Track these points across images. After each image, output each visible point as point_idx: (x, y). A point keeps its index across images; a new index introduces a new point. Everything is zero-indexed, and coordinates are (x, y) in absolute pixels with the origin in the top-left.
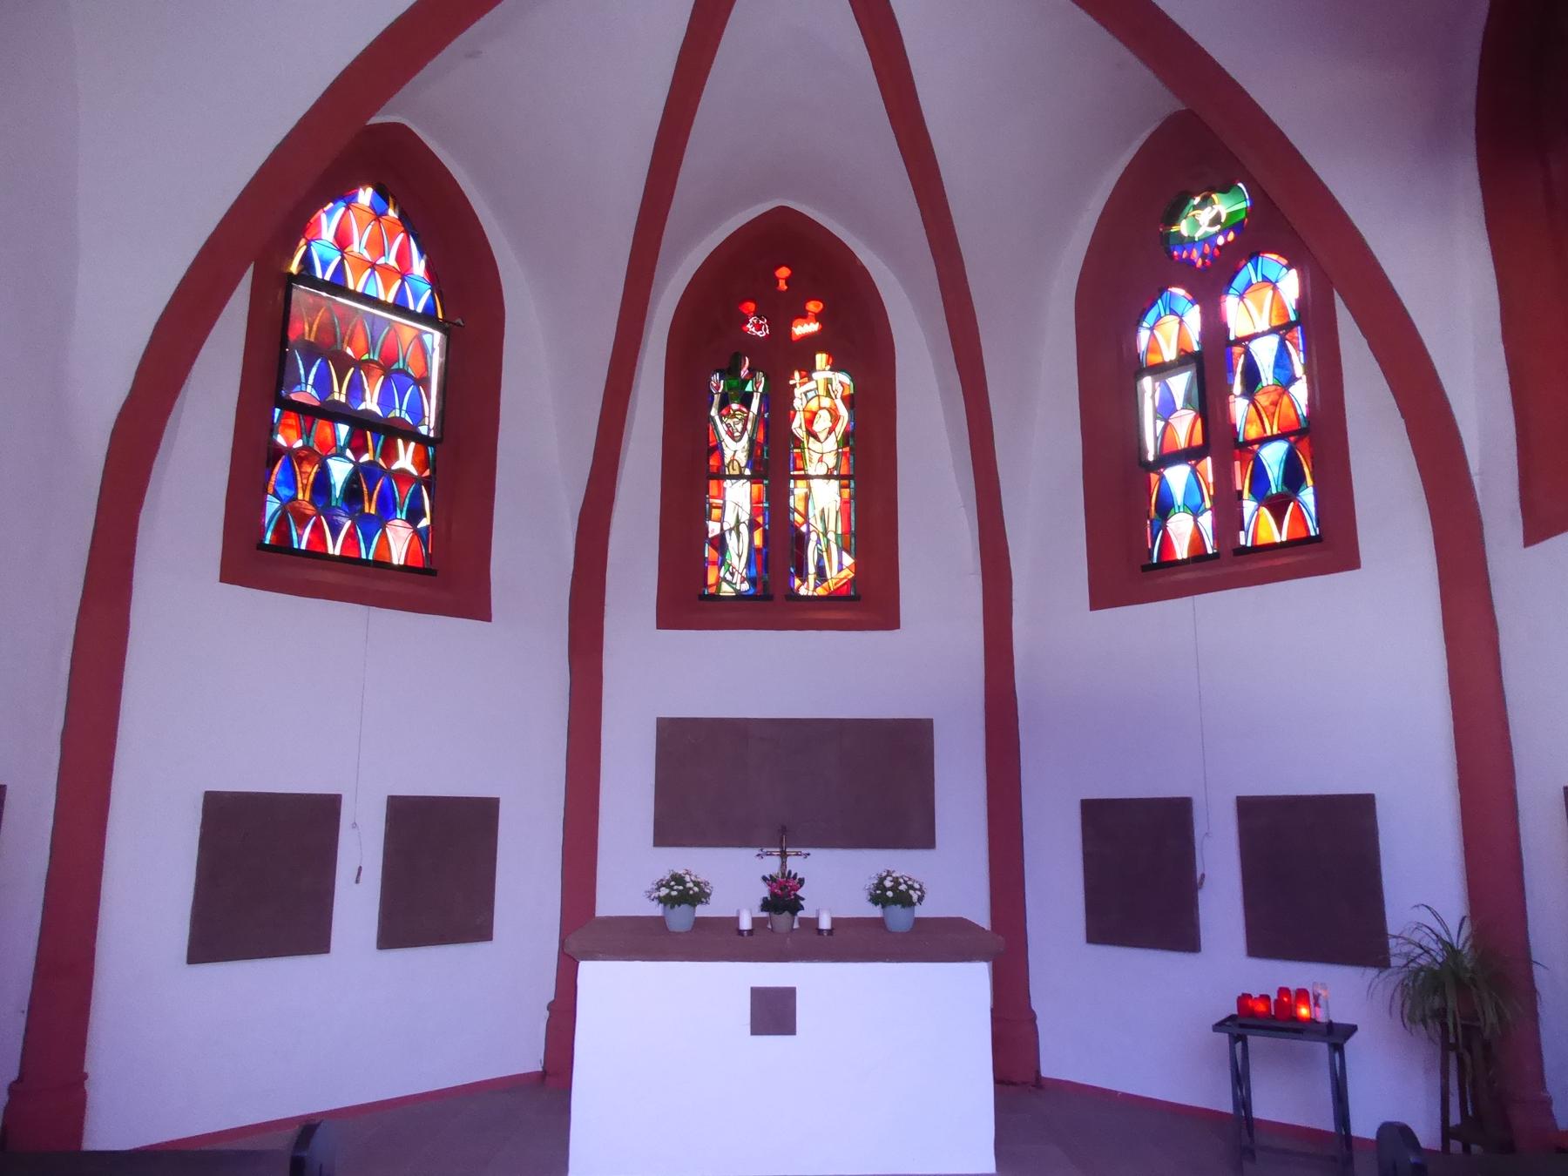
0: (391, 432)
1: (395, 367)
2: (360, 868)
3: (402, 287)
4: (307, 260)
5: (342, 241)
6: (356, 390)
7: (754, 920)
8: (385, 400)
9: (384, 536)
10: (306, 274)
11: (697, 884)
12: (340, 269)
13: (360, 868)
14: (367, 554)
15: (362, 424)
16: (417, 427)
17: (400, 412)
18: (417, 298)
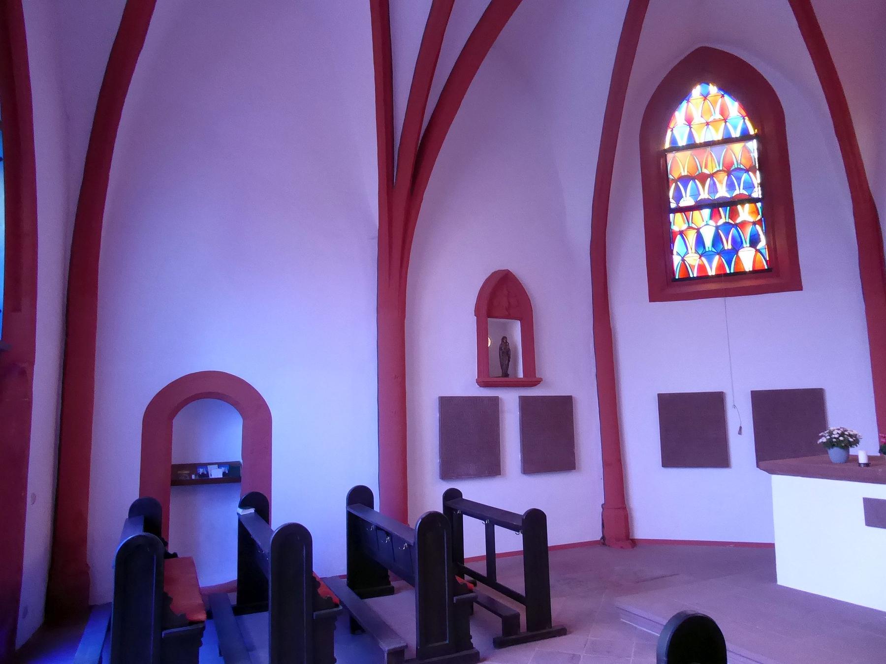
0: (731, 204)
1: (733, 168)
2: (741, 428)
3: (726, 126)
4: (674, 141)
5: (689, 121)
6: (714, 189)
7: (870, 458)
8: (731, 186)
9: (738, 258)
10: (675, 148)
11: (850, 436)
12: (691, 135)
13: (741, 428)
14: (730, 270)
15: (715, 206)
16: (751, 195)
17: (739, 191)
18: (735, 128)
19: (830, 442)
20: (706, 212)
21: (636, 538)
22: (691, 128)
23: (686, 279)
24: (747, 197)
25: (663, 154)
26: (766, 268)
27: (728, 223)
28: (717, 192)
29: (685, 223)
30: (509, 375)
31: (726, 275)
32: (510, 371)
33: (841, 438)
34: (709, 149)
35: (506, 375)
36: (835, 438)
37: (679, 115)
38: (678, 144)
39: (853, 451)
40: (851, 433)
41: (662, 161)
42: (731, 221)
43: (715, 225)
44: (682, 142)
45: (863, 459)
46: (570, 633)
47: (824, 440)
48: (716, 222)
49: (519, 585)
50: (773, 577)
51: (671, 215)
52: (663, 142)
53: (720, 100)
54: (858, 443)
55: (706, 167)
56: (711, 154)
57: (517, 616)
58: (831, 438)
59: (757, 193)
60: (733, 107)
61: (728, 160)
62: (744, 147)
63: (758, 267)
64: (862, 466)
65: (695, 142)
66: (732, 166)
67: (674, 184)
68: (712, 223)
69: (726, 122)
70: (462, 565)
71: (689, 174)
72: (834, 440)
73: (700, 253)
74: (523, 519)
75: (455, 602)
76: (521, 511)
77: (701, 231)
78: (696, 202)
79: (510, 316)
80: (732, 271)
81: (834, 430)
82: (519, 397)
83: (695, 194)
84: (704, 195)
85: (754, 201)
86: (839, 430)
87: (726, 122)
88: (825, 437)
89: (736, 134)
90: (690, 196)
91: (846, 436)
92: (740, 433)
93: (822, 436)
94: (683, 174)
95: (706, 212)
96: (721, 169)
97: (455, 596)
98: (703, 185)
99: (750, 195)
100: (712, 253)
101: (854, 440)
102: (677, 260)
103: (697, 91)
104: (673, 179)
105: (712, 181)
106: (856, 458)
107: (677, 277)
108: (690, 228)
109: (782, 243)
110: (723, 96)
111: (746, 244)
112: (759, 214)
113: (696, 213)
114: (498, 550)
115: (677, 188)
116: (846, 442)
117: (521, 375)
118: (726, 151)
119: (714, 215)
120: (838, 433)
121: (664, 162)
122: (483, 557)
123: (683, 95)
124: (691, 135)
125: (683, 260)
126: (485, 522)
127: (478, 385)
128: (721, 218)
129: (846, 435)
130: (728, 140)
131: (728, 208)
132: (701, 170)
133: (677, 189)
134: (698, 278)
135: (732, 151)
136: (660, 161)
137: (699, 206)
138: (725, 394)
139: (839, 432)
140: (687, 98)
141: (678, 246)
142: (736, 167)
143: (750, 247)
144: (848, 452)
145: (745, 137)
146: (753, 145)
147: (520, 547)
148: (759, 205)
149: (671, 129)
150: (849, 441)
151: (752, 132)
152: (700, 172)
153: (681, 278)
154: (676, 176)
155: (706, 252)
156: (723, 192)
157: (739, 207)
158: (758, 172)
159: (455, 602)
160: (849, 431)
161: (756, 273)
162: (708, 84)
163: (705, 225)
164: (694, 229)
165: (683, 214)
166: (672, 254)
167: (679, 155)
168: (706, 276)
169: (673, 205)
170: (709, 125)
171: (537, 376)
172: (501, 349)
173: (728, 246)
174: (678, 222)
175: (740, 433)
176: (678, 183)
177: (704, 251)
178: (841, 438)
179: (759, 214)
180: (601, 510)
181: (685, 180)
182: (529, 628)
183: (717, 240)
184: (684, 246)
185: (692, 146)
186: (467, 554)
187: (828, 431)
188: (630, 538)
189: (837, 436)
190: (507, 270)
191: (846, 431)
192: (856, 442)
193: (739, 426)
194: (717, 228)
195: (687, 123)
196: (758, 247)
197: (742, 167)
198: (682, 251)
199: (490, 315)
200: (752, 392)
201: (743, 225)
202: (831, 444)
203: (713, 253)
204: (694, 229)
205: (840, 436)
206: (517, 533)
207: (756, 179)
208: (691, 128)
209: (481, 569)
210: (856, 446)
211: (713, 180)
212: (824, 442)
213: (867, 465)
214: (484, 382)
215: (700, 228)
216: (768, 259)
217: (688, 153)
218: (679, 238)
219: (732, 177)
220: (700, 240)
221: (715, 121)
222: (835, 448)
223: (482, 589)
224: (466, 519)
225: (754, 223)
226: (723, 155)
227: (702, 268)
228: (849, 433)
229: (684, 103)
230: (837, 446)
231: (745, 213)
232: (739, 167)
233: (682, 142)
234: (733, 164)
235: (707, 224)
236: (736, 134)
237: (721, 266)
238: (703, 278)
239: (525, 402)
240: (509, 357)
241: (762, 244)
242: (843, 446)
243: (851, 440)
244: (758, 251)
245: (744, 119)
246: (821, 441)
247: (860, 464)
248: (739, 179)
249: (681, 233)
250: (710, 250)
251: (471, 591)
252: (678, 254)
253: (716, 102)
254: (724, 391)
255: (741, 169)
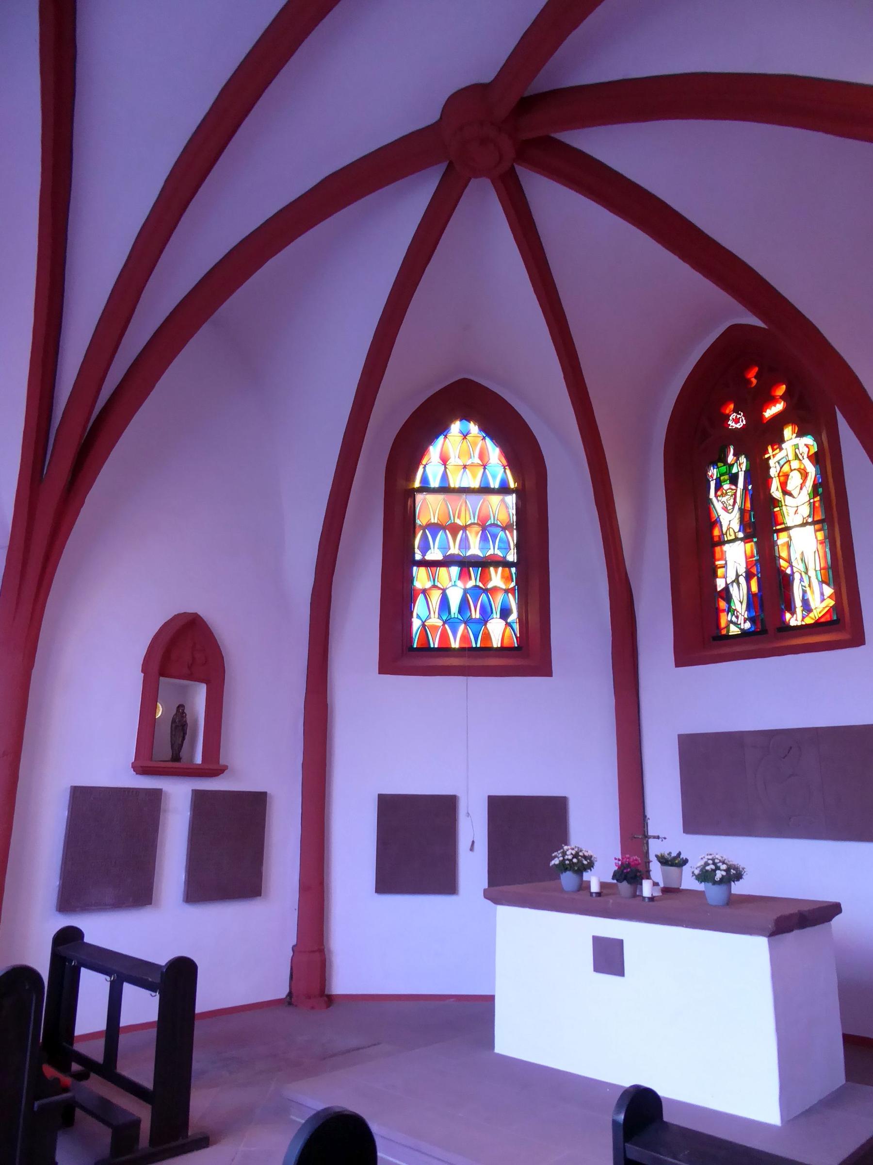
0: (484, 564)
2: (473, 842)
4: (425, 479)
5: (444, 460)
7: (603, 885)
10: (425, 489)
11: (585, 857)
12: (445, 476)
13: (473, 842)
14: (476, 644)
15: (466, 564)
18: (494, 477)
19: (563, 865)
20: (455, 570)
21: (333, 993)
22: (446, 468)
23: (425, 649)
24: (501, 559)
25: (411, 493)
26: (516, 645)
27: (478, 587)
28: (469, 548)
29: (429, 579)
30: (181, 759)
31: (471, 649)
32: (184, 753)
33: (575, 860)
34: (464, 496)
35: (176, 758)
36: (568, 859)
37: (434, 451)
38: (430, 485)
39: (586, 876)
40: (586, 854)
41: (410, 502)
42: (481, 585)
43: (463, 588)
44: (434, 483)
45: (595, 888)
46: (215, 1143)
47: (556, 861)
48: (465, 585)
49: (145, 1077)
50: (489, 1040)
51: (415, 568)
52: (414, 481)
53: (480, 443)
54: (593, 867)
55: (459, 517)
56: (466, 503)
57: (137, 1123)
58: (564, 860)
59: (512, 557)
60: (494, 453)
61: (484, 511)
62: (503, 501)
63: (507, 643)
64: (594, 895)
65: (449, 484)
66: (487, 520)
67: (421, 532)
68: (460, 584)
69: (485, 469)
70: (70, 1047)
71: (439, 522)
72: (567, 862)
73: (444, 618)
74: (162, 973)
75: (36, 1109)
76: (162, 959)
77: (448, 591)
78: (445, 557)
79: (191, 676)
80: (478, 645)
81: (568, 850)
82: (192, 790)
83: (445, 548)
84: (454, 550)
85: (507, 564)
86: (573, 849)
87: (485, 469)
88: (558, 858)
89: (495, 484)
90: (438, 548)
91: (580, 857)
92: (472, 849)
93: (556, 857)
94: (432, 521)
95: (455, 570)
96: (476, 522)
97: (37, 1100)
98: (454, 538)
99: (505, 558)
100: (457, 621)
101: (588, 863)
102: (416, 624)
103: (456, 427)
104: (420, 525)
105: (464, 534)
106: (588, 885)
107: (415, 646)
108: (434, 586)
109: (534, 619)
110: (484, 438)
111: (496, 614)
112: (512, 581)
113: (443, 571)
114: (124, 1022)
115: (424, 536)
116: (580, 864)
117: (198, 759)
118: (483, 503)
119: (464, 575)
120: (572, 854)
121: (412, 503)
122: (154, 1022)
123: (442, 429)
124: (445, 476)
125: (424, 625)
126: (111, 979)
127: (134, 771)
128: (470, 578)
129: (580, 856)
130: (485, 490)
131: (480, 569)
132: (454, 520)
133: (424, 537)
134: (481, 649)
135: (489, 503)
136: (408, 501)
137: (446, 563)
138: (458, 797)
139: (574, 852)
140: (445, 434)
141: (419, 607)
142: (493, 522)
143: (500, 618)
144: (582, 876)
145: (504, 489)
146: (511, 500)
147: (153, 1015)
148: (513, 570)
149: (423, 466)
150: (583, 864)
151: (512, 485)
152: (452, 522)
153: (483, 647)
154: (424, 523)
155: (451, 618)
156: (475, 549)
157: (492, 569)
158: (515, 532)
159: (36, 1109)
160: (583, 852)
161: (504, 650)
162: (470, 422)
163: (452, 586)
164: (440, 589)
165: (429, 568)
166: (412, 616)
167: (430, 498)
168: (447, 648)
169: (418, 556)
170: (466, 468)
171: (222, 761)
172: (173, 721)
173: (476, 615)
174: (421, 578)
175: (472, 849)
176: (427, 531)
177: (449, 617)
178: (575, 860)
179: (512, 581)
180: (291, 954)
181: (434, 528)
182: (153, 1141)
183: (464, 605)
184: (427, 608)
185: (444, 489)
186: (81, 1029)
187: (562, 850)
188: (326, 993)
189: (570, 857)
190: (196, 613)
191: (581, 851)
192: (591, 866)
193: (472, 841)
194: (466, 591)
195: (442, 463)
196: (509, 620)
197: (499, 523)
198: (424, 614)
199: (163, 673)
200: (489, 797)
201: (495, 589)
202: (564, 867)
203: (459, 621)
204: (440, 589)
205: (573, 858)
206: (153, 994)
207: (512, 538)
208: (446, 468)
209: (96, 1051)
210: (591, 870)
211: (466, 534)
212: (557, 865)
213: (599, 894)
214: (142, 768)
215: (446, 589)
216: (518, 635)
217: (440, 497)
218: (421, 598)
219: (487, 531)
220: (445, 603)
221: (472, 465)
222: (568, 873)
223: (96, 1086)
224: (86, 974)
225: (507, 591)
226: (478, 508)
227: (444, 636)
228: (583, 854)
229: (441, 438)
230: (570, 870)
231: (497, 578)
232: (496, 522)
233: (434, 483)
234: (488, 518)
235: (455, 585)
236: (495, 484)
237: (465, 638)
238: (445, 650)
239: (199, 797)
240: (185, 734)
241: (513, 617)
242: (576, 871)
243: (585, 862)
244: (508, 624)
245: (505, 469)
246: (553, 863)
247: (591, 894)
248: (494, 537)
249: (424, 592)
250: (456, 616)
251: (66, 1089)
252: (418, 617)
253: (475, 444)
254: (458, 795)
255: (497, 526)
